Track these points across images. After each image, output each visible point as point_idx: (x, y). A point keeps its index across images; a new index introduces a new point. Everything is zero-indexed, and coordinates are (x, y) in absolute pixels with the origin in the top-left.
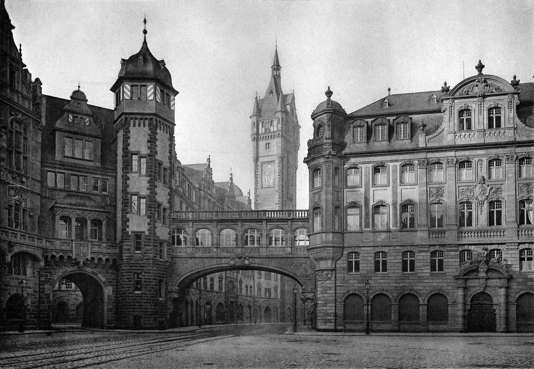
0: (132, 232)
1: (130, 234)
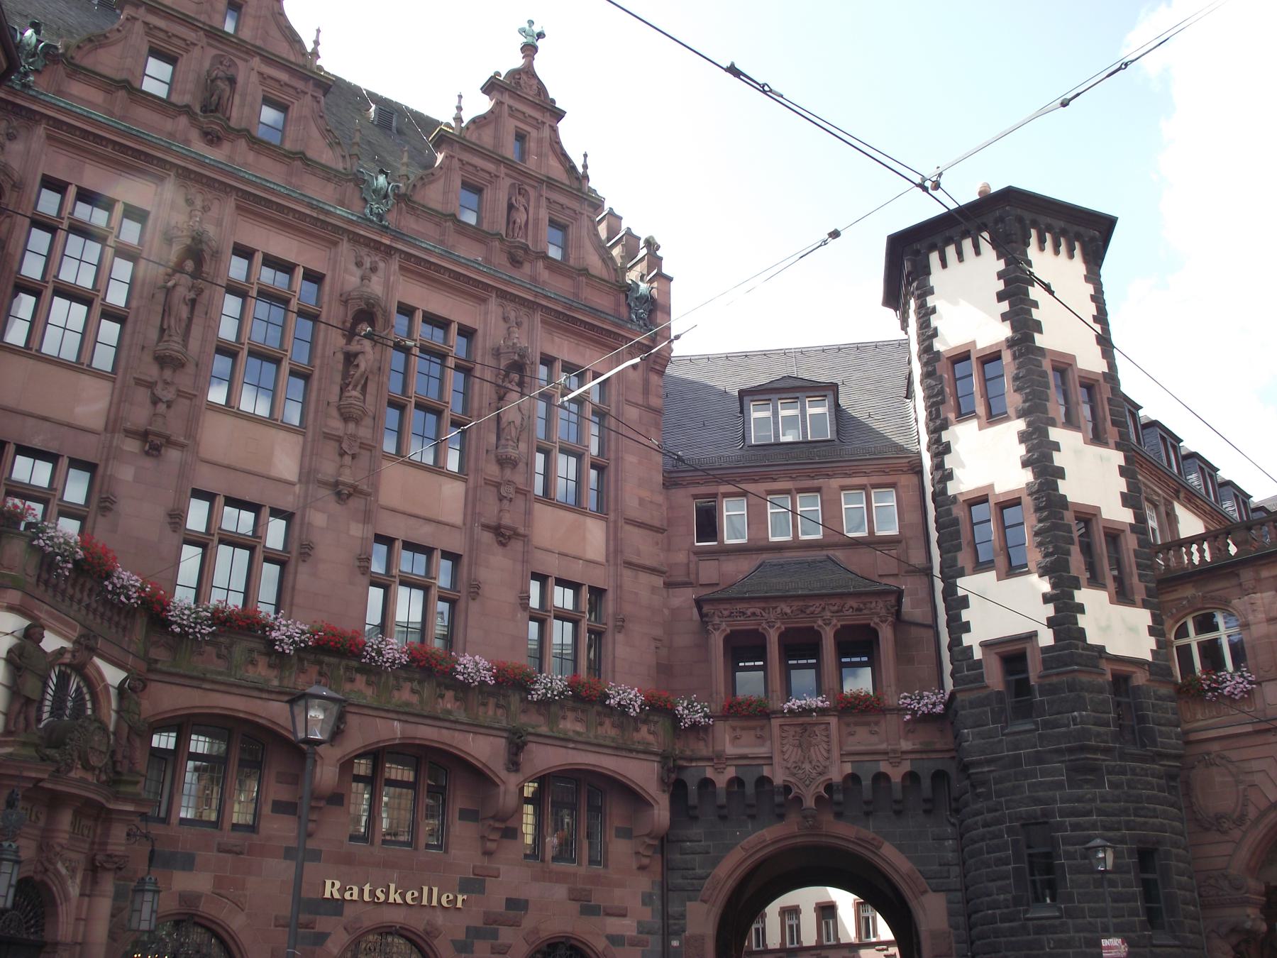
0: (985, 645)
1: (978, 654)
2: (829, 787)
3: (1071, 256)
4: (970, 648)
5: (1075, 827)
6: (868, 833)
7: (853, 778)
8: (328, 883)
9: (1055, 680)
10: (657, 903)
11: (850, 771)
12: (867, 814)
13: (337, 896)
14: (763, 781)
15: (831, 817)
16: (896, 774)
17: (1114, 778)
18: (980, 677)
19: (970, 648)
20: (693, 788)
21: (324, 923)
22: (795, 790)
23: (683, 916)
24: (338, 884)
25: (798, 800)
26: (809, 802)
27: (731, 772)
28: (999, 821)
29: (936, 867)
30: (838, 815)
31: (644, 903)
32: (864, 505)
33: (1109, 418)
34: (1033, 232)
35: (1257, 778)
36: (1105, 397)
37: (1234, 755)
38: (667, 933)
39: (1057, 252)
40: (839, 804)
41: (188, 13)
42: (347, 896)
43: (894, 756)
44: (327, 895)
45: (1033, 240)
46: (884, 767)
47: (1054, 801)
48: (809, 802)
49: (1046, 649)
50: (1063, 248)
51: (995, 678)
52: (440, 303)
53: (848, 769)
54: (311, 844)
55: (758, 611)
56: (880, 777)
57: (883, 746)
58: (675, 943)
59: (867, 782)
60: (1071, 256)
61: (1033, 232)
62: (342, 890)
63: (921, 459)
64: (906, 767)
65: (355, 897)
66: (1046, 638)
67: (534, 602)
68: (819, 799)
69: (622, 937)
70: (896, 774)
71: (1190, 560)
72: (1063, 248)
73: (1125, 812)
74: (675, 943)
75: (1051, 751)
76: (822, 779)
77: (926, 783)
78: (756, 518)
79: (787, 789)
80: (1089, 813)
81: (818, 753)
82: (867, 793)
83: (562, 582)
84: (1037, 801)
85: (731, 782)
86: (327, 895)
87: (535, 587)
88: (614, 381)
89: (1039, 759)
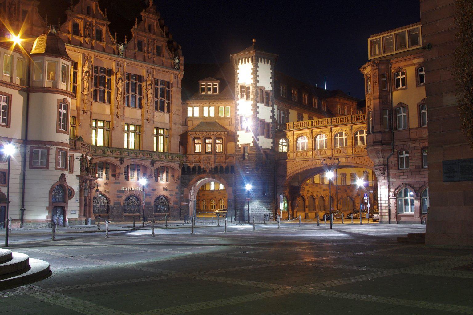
0: (241, 145)
1: (240, 146)
2: (212, 168)
3: (268, 64)
4: (239, 145)
8: (122, 188)
10: (179, 189)
11: (216, 165)
13: (123, 190)
14: (199, 167)
16: (224, 166)
19: (239, 145)
20: (186, 168)
21: (122, 194)
22: (205, 169)
23: (184, 191)
24: (123, 188)
25: (206, 171)
27: (193, 165)
31: (176, 189)
32: (223, 110)
33: (270, 100)
34: (260, 59)
36: (270, 96)
38: (181, 194)
39: (264, 63)
41: (214, 246)
42: (125, 190)
44: (122, 190)
45: (260, 62)
50: (266, 62)
52: (130, 65)
54: (117, 181)
55: (199, 134)
58: (182, 196)
60: (268, 64)
61: (260, 59)
62: (124, 189)
65: (126, 190)
67: (155, 133)
68: (210, 170)
69: (96, 136)
70: (224, 166)
71: (315, 100)
72: (266, 62)
74: (182, 196)
76: (210, 167)
78: (201, 111)
83: (160, 128)
85: (193, 167)
86: (122, 190)
87: (155, 131)
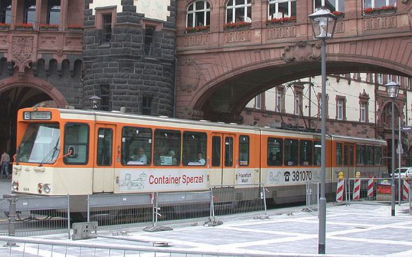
0: (97, 9)
1: (94, 14)
2: (31, 64)
5: (119, 88)
6: (47, 84)
7: (41, 61)
9: (120, 27)
12: (48, 76)
15: (33, 76)
16: (60, 60)
17: (137, 69)
18: (93, 23)
25: (17, 68)
26: (21, 70)
28: (91, 83)
29: (73, 99)
30: (36, 75)
35: (203, 72)
37: (197, 62)
40: (35, 71)
43: (61, 53)
46: (55, 57)
47: (113, 77)
48: (21, 70)
49: (120, 14)
51: (99, 24)
53: (40, 56)
56: (53, 61)
57: (56, 48)
59: (47, 63)
63: (177, 117)
64: (65, 57)
66: (120, 10)
68: (26, 68)
73: (141, 83)
75: (114, 57)
77: (72, 64)
79: (13, 63)
80: (125, 82)
81: (28, 50)
82: (59, 68)
84: (107, 77)
85: (64, 61)
88: (189, 100)
89: (109, 59)
